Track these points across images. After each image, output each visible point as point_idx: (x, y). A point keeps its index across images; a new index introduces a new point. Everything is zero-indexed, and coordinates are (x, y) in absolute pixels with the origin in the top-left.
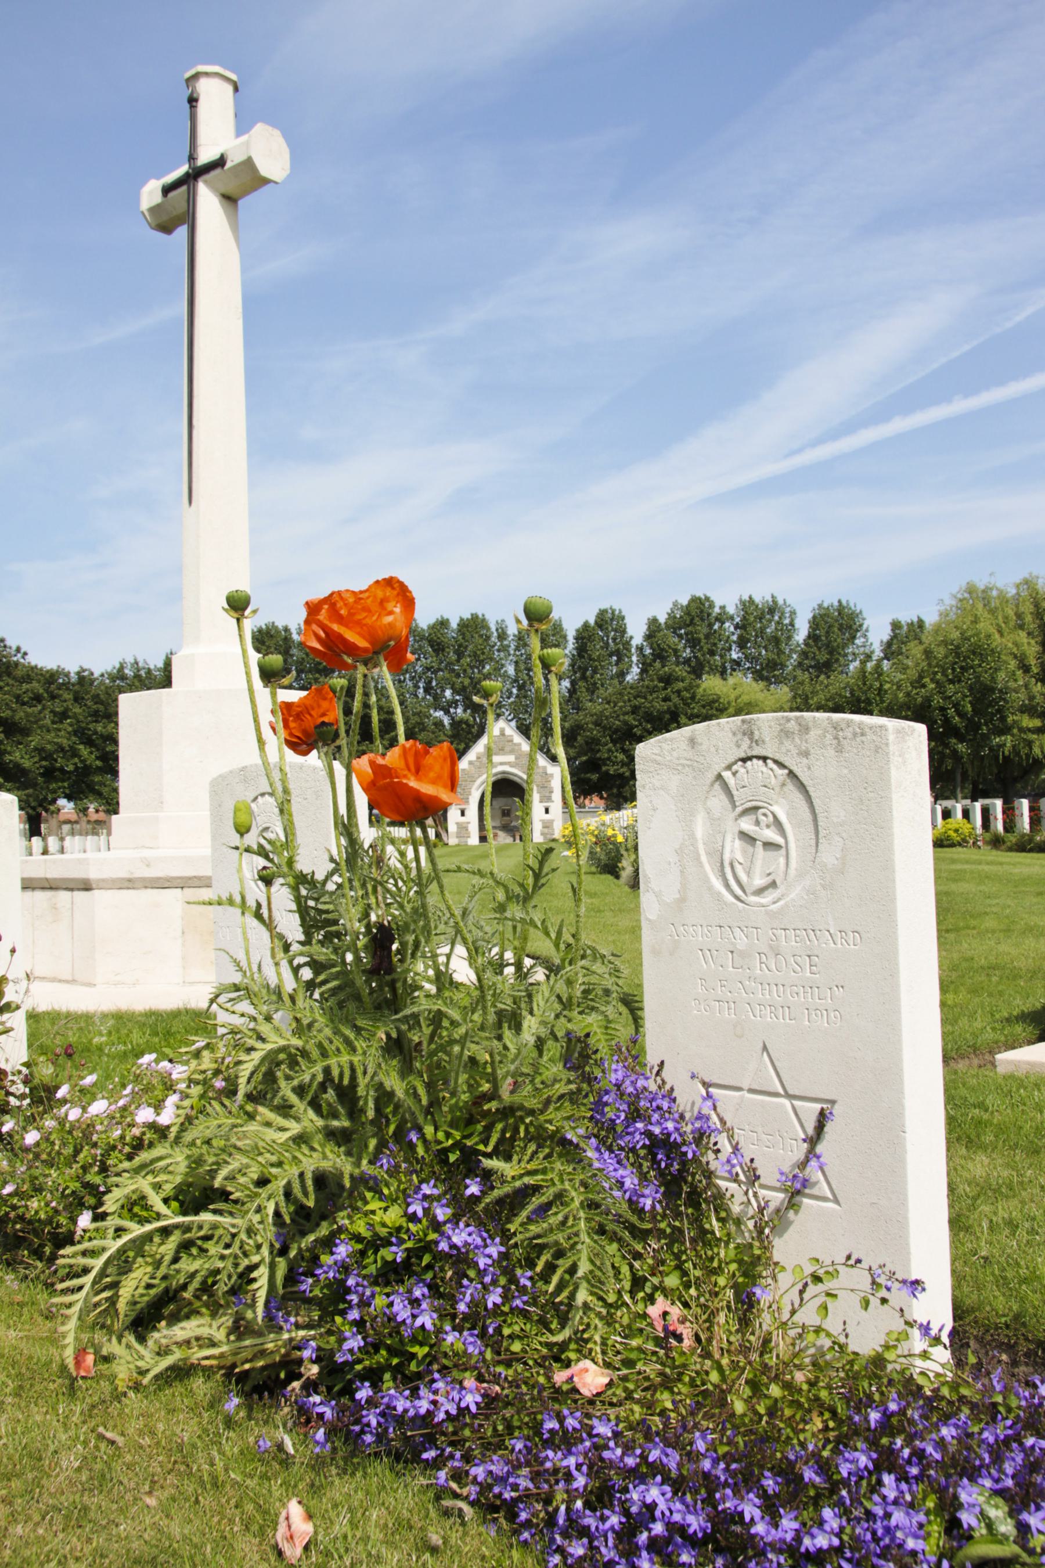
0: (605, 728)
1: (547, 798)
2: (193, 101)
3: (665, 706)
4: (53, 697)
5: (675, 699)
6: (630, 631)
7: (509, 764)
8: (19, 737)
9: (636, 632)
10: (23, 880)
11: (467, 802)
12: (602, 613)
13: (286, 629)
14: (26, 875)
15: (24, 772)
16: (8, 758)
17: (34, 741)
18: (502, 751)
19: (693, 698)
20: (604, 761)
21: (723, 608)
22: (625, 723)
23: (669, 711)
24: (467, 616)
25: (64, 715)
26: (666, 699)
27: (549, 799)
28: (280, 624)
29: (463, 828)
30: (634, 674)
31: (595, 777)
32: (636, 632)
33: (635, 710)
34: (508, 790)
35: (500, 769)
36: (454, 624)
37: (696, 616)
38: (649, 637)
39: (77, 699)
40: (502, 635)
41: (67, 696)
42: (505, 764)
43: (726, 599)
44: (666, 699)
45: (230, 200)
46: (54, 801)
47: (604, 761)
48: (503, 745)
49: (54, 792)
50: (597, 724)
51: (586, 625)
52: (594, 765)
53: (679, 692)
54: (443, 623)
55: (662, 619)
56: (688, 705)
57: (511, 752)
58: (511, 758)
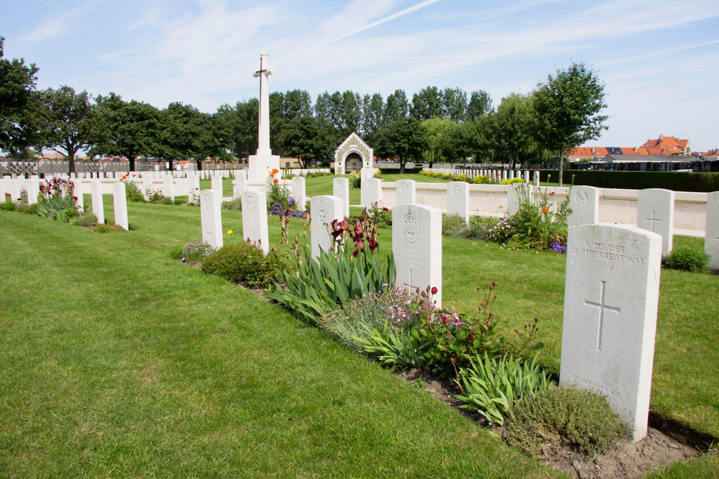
0: (387, 137)
1: (368, 160)
2: (261, 59)
3: (408, 130)
4: (206, 123)
5: (411, 128)
6: (407, 98)
7: (356, 148)
8: (196, 137)
9: (409, 99)
10: (90, 195)
11: (341, 160)
12: (397, 91)
13: (282, 94)
14: (104, 193)
15: (197, 148)
16: (193, 144)
17: (201, 139)
18: (353, 143)
19: (417, 128)
20: (387, 148)
21: (441, 91)
22: (394, 135)
23: (409, 132)
24: (346, 92)
25: (210, 129)
26: (409, 128)
27: (369, 160)
28: (279, 92)
29: (340, 169)
30: (408, 114)
31: (384, 153)
32: (409, 99)
33: (398, 131)
34: (354, 157)
35: (353, 149)
36: (342, 93)
37: (430, 95)
38: (414, 101)
39: (213, 123)
40: (358, 98)
41: (211, 122)
42: (354, 148)
43: (441, 88)
44: (409, 128)
45: (267, 75)
46: (206, 157)
47: (387, 148)
48: (353, 142)
49: (206, 154)
50: (385, 135)
51: (392, 95)
52: (383, 149)
53: (413, 126)
54: (338, 93)
55: (418, 94)
56: (416, 130)
57: (356, 144)
58: (356, 146)
